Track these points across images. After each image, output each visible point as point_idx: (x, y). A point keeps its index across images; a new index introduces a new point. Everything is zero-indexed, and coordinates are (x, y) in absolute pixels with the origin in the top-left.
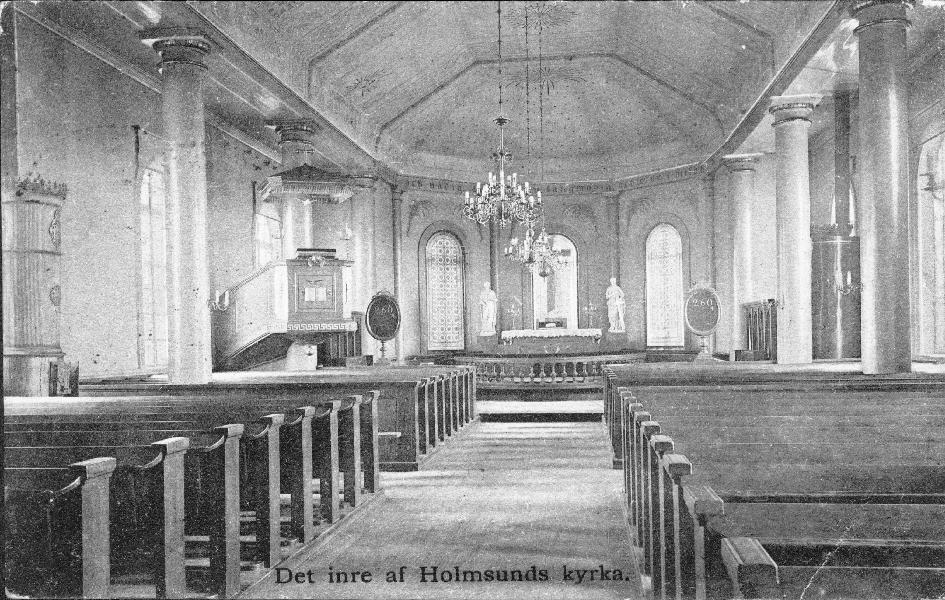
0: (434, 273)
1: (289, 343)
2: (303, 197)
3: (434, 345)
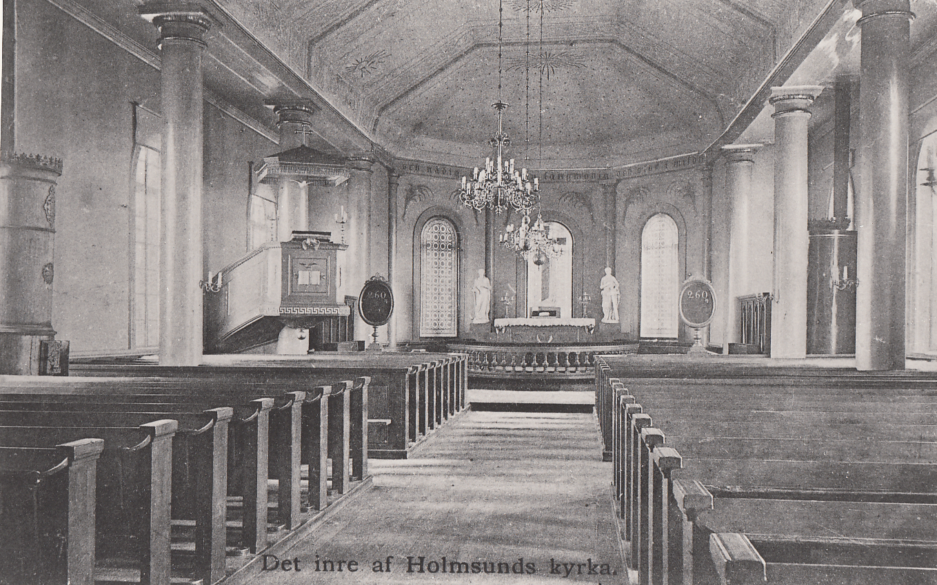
0: (429, 258)
1: (281, 327)
2: (300, 179)
3: (426, 332)
